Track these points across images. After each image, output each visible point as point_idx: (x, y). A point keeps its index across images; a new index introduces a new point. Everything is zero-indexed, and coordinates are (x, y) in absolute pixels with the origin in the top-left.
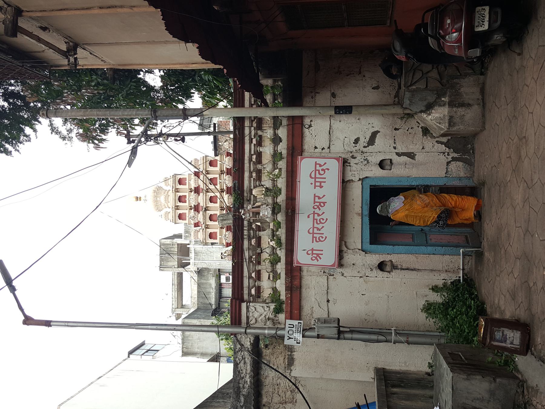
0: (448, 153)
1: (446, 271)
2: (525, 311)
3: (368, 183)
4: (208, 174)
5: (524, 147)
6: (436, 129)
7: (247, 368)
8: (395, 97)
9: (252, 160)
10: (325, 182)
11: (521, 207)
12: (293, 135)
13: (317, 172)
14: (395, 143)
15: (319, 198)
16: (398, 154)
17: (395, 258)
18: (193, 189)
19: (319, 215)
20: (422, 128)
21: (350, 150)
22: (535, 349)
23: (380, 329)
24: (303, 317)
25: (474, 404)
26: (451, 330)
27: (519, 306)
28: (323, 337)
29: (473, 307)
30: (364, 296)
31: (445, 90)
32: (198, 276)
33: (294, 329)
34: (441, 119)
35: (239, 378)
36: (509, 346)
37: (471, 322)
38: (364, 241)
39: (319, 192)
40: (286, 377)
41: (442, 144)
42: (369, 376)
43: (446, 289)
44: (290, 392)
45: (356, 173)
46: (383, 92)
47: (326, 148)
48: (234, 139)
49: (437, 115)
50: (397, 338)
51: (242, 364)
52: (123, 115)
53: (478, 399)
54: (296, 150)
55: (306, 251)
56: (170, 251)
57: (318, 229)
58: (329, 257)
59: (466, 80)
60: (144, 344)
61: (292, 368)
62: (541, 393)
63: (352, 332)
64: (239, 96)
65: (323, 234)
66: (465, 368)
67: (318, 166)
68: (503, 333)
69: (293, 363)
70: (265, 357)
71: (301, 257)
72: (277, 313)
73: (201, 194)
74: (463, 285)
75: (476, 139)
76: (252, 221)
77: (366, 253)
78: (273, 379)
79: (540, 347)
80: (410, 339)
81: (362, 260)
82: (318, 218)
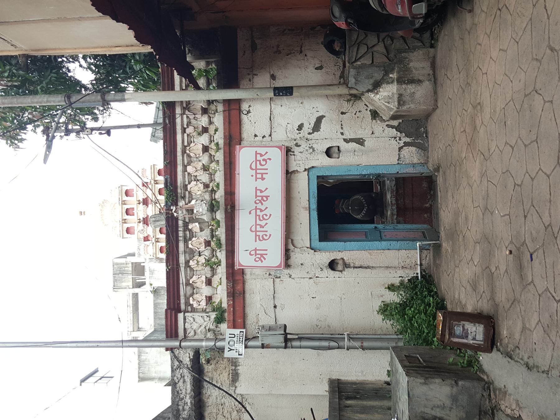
0: (400, 138)
1: (403, 267)
2: (488, 301)
3: (314, 174)
4: (157, 183)
5: (479, 114)
6: (385, 110)
7: (186, 388)
8: (340, 77)
9: (186, 153)
10: (267, 173)
11: (478, 182)
12: (230, 123)
13: (258, 162)
14: (342, 128)
15: (261, 191)
16: (346, 141)
17: (347, 256)
18: (141, 200)
19: (261, 211)
20: (370, 111)
21: (293, 137)
22: (501, 344)
23: (331, 334)
24: (248, 326)
25: (434, 413)
26: (409, 331)
27: (481, 297)
28: (268, 347)
29: (432, 304)
30: (314, 299)
31: (393, 66)
32: (154, 296)
33: (235, 339)
34: (390, 98)
35: (177, 400)
36: (471, 342)
37: (430, 321)
38: (312, 238)
39: (261, 185)
40: (231, 395)
41: (393, 128)
42: (323, 389)
43: (403, 288)
44: (236, 412)
45: (301, 162)
46: (327, 73)
47: (267, 136)
48: (164, 127)
49: (386, 94)
50: (351, 344)
51: (181, 384)
52: (33, 103)
53: (438, 407)
54: (233, 139)
55: (249, 252)
56: (124, 271)
57: (261, 227)
58: (275, 257)
59: (415, 53)
60: (98, 371)
61: (237, 384)
62: (510, 395)
63: (300, 339)
64: (168, 81)
65: (267, 231)
66: (421, 370)
67: (258, 156)
68: (464, 329)
69: (238, 378)
70: (206, 374)
71: (243, 258)
72: (218, 323)
73: (150, 206)
74: (421, 282)
75: (429, 121)
76: (187, 220)
77: (315, 251)
78: (217, 398)
79: (506, 341)
80: (365, 344)
81: (312, 258)
82: (261, 214)
